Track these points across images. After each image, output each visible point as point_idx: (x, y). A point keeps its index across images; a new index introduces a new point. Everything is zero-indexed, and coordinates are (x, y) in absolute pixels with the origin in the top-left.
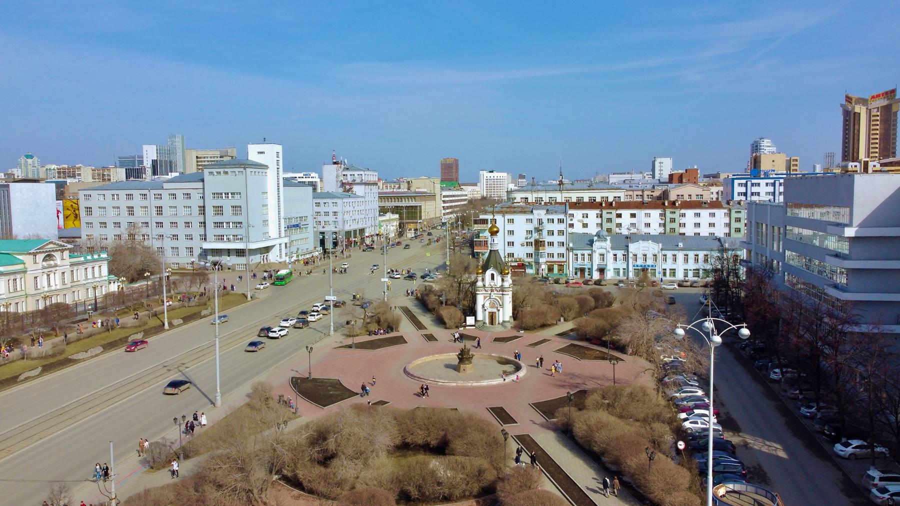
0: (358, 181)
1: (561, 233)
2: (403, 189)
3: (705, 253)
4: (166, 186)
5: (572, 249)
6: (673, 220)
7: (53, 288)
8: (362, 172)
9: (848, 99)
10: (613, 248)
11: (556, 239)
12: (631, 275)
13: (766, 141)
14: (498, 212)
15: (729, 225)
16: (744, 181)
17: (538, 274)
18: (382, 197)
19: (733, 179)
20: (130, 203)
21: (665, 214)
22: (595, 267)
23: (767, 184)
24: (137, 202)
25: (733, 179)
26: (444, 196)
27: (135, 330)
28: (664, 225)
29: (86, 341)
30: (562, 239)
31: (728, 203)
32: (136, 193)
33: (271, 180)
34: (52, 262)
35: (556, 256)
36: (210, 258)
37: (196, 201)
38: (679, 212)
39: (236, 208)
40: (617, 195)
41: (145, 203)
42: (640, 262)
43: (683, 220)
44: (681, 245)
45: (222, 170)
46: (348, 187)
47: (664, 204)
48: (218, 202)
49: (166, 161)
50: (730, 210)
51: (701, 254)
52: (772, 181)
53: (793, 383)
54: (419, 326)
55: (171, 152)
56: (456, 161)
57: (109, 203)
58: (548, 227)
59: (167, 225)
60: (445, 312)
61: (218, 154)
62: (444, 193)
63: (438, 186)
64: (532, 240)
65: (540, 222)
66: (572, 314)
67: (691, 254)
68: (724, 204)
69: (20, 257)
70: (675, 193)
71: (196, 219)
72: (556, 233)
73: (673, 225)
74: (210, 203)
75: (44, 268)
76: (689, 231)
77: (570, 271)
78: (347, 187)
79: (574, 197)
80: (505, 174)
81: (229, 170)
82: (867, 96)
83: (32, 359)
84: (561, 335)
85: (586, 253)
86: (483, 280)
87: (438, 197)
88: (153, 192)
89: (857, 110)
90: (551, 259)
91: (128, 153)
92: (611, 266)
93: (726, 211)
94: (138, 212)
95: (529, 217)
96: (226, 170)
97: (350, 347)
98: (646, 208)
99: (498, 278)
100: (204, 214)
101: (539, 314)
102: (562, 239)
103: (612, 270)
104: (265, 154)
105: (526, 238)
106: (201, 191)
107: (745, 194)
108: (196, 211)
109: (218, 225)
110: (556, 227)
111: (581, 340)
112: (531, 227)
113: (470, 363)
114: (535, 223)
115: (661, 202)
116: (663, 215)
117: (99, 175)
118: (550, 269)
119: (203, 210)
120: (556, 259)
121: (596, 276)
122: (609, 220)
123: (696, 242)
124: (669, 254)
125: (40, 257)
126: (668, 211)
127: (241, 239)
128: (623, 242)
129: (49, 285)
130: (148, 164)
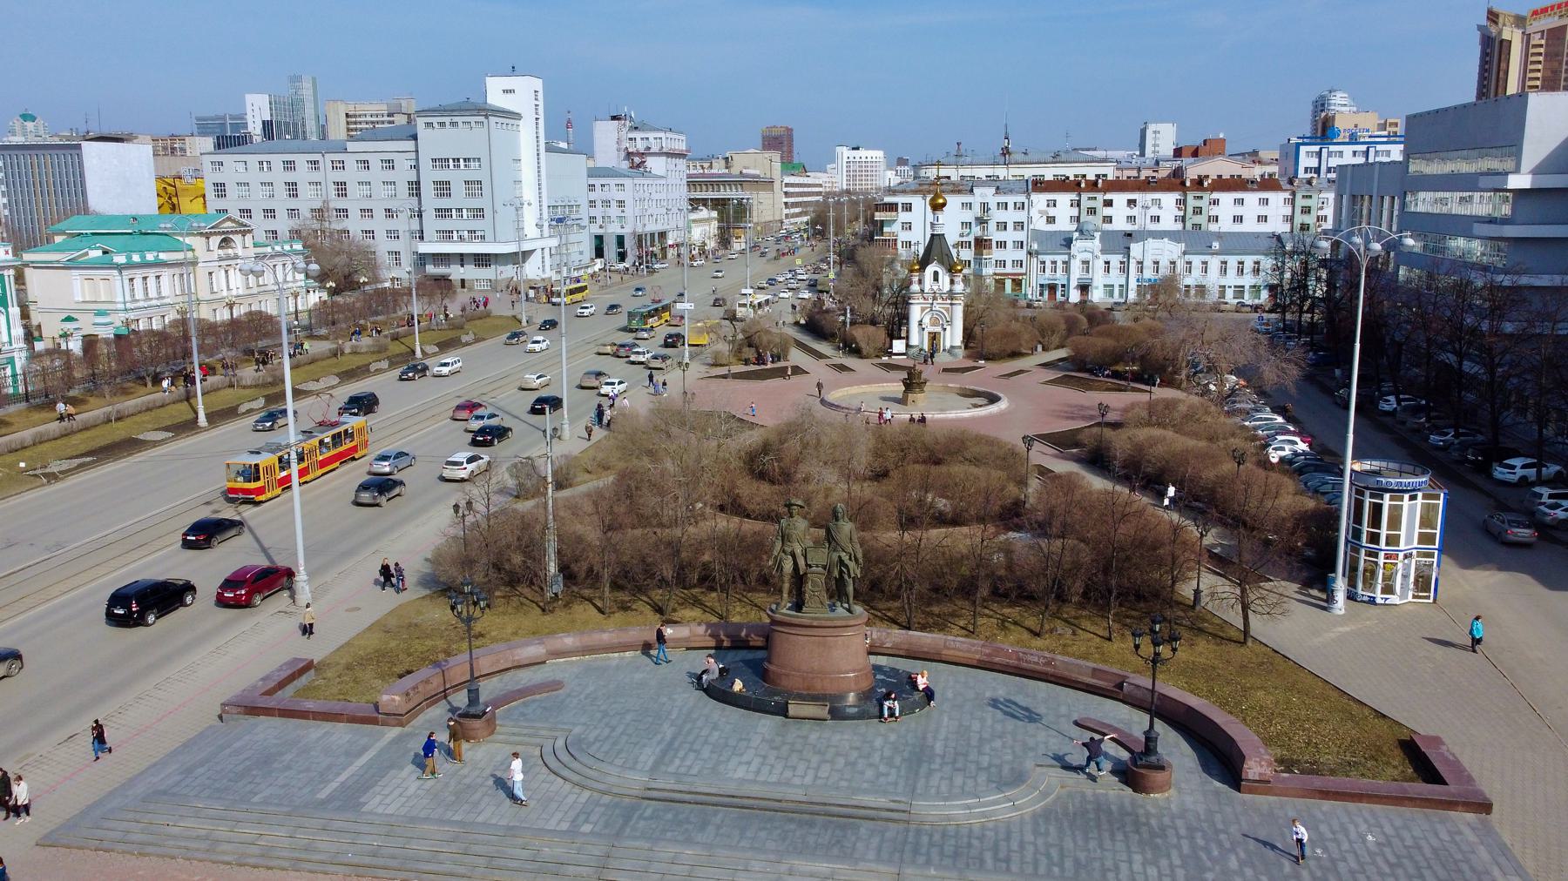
0: (655, 149)
1: (1019, 225)
2: (718, 168)
3: (1256, 258)
4: (351, 146)
5: (1037, 253)
6: (1198, 211)
7: (234, 293)
8: (661, 135)
9: (1493, 16)
10: (1104, 251)
11: (1010, 236)
12: (1132, 296)
13: (1339, 94)
14: (915, 192)
15: (1291, 219)
16: (1316, 148)
17: (979, 294)
18: (692, 184)
19: (1298, 145)
20: (290, 177)
21: (1185, 201)
22: (1074, 283)
23: (1355, 153)
24: (302, 174)
25: (1298, 145)
26: (787, 185)
27: (375, 357)
28: (1183, 219)
29: (307, 368)
30: (1021, 236)
31: (1291, 182)
32: (301, 160)
33: (527, 137)
34: (230, 251)
35: (1009, 264)
36: (431, 269)
37: (403, 174)
38: (1208, 196)
39: (473, 186)
40: (1101, 171)
41: (316, 176)
42: (1149, 274)
43: (1214, 211)
44: (1216, 245)
45: (447, 120)
46: (637, 160)
47: (1183, 183)
48: (442, 175)
49: (287, 124)
50: (1294, 194)
51: (1249, 261)
52: (1364, 148)
53: (1416, 411)
54: (819, 356)
55: (295, 105)
56: (789, 130)
57: (255, 176)
58: (997, 215)
59: (354, 213)
60: (860, 334)
61: (384, 109)
62: (788, 180)
63: (777, 166)
64: (971, 238)
65: (985, 207)
66: (1056, 339)
67: (1233, 261)
68: (1284, 183)
69: (188, 240)
70: (1193, 171)
71: (405, 202)
72: (1010, 226)
73: (1198, 219)
74: (429, 176)
75: (221, 259)
76: (1226, 225)
77: (1031, 291)
78: (636, 161)
79: (1029, 172)
80: (880, 154)
81: (459, 120)
82: (1525, 12)
83: (244, 387)
84: (1045, 365)
85: (1060, 259)
86: (920, 282)
87: (777, 185)
88: (329, 157)
89: (1506, 36)
90: (1000, 270)
91: (214, 109)
92: (1099, 280)
93: (1287, 195)
94: (305, 191)
95: (967, 199)
96: (455, 119)
97: (724, 377)
98: (1155, 190)
99: (945, 279)
100: (419, 195)
101: (1006, 335)
102: (1021, 236)
103: (1101, 288)
104: (516, 93)
105: (962, 235)
106: (413, 155)
107: (1317, 170)
108: (403, 189)
109: (443, 213)
110: (1011, 216)
111: (1079, 371)
112: (969, 216)
113: (922, 391)
114: (977, 211)
115: (1175, 182)
116: (1182, 203)
117: (165, 148)
118: (1000, 283)
119: (416, 188)
120: (1009, 269)
121: (1075, 297)
122: (1092, 211)
123: (1235, 244)
124: (1196, 260)
125: (215, 241)
126: (1190, 196)
127: (483, 237)
128: (1122, 242)
129: (228, 289)
130: (255, 129)
